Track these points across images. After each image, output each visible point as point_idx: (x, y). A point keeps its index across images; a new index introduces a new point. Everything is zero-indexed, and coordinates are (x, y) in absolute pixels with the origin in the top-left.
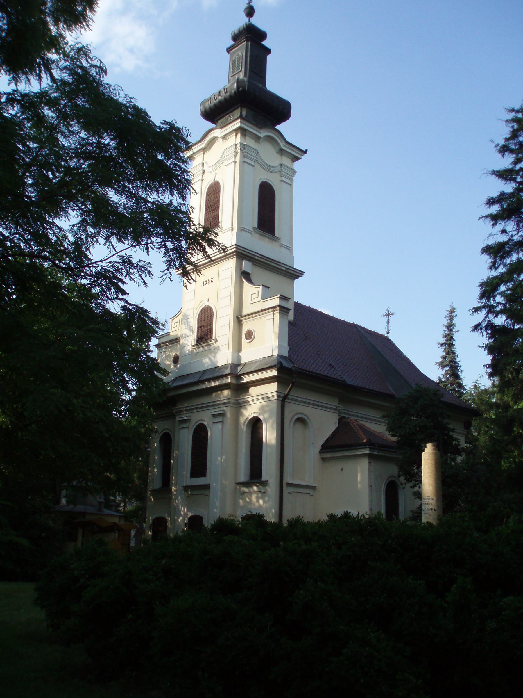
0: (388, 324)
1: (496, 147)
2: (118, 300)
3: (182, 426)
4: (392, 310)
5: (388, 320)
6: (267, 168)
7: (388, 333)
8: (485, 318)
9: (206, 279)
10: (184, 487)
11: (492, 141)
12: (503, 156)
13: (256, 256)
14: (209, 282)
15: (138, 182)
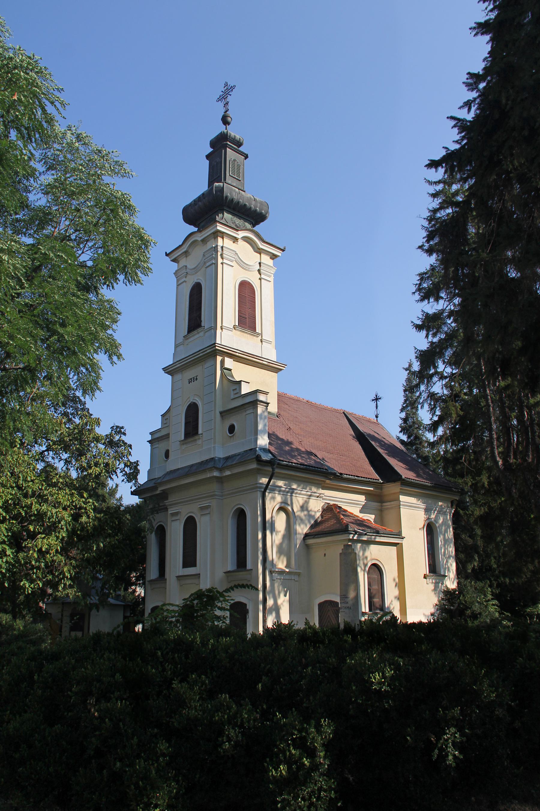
0: (377, 408)
3: (174, 518)
4: (380, 395)
5: (377, 404)
7: (377, 417)
10: (177, 577)
13: (236, 352)
14: (194, 380)
15: (465, 272)
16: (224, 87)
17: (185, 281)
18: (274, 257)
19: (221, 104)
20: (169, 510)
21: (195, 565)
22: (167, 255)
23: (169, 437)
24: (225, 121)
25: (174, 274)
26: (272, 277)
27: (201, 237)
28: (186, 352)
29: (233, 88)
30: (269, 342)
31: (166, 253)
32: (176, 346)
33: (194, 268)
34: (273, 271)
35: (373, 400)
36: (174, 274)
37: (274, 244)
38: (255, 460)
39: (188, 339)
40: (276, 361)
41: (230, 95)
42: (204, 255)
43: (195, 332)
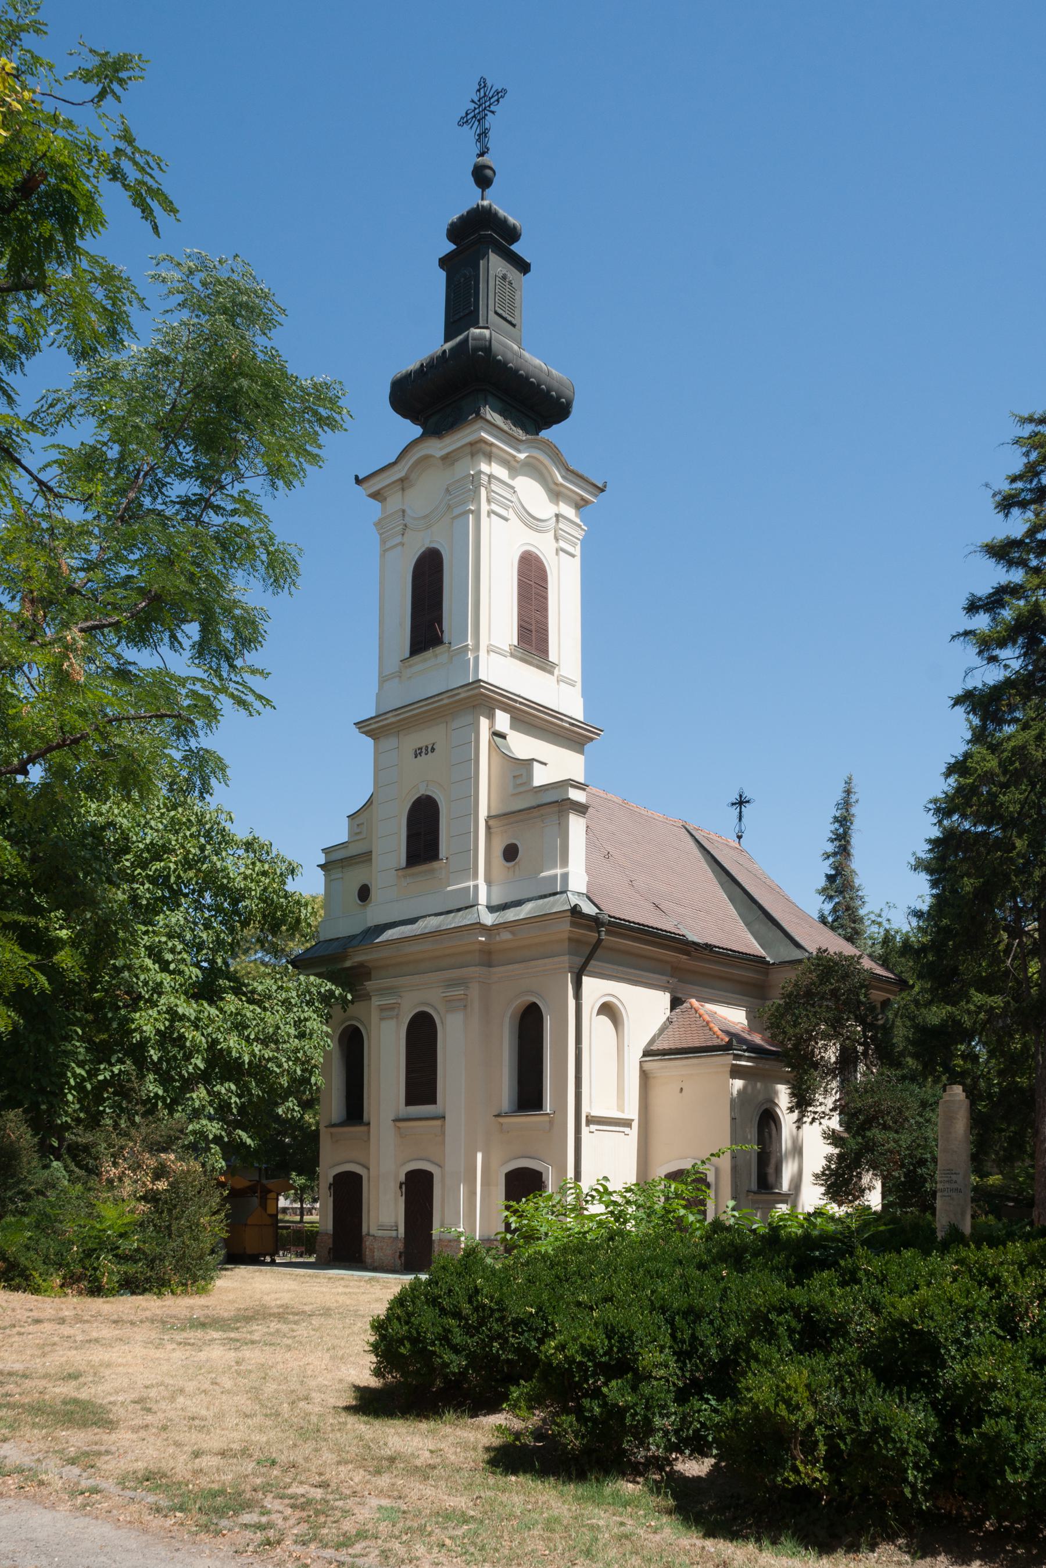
0: (740, 820)
1: (994, 495)
2: (846, 954)
4: (748, 795)
5: (740, 812)
6: (532, 522)
8: (155, 224)
9: (422, 744)
11: (987, 485)
12: (1006, 516)
16: (479, 90)
17: (402, 544)
18: (582, 503)
19: (469, 133)
20: (373, 999)
21: (433, 1101)
22: (358, 481)
23: (370, 860)
24: (482, 178)
25: (375, 524)
26: (578, 547)
27: (441, 449)
28: (400, 695)
29: (501, 94)
30: (572, 684)
31: (357, 477)
32: (383, 680)
33: (425, 517)
34: (579, 534)
35: (733, 804)
36: (375, 524)
37: (586, 475)
38: (569, 914)
39: (410, 666)
40: (582, 720)
41: (493, 112)
42: (447, 490)
43: (429, 654)
